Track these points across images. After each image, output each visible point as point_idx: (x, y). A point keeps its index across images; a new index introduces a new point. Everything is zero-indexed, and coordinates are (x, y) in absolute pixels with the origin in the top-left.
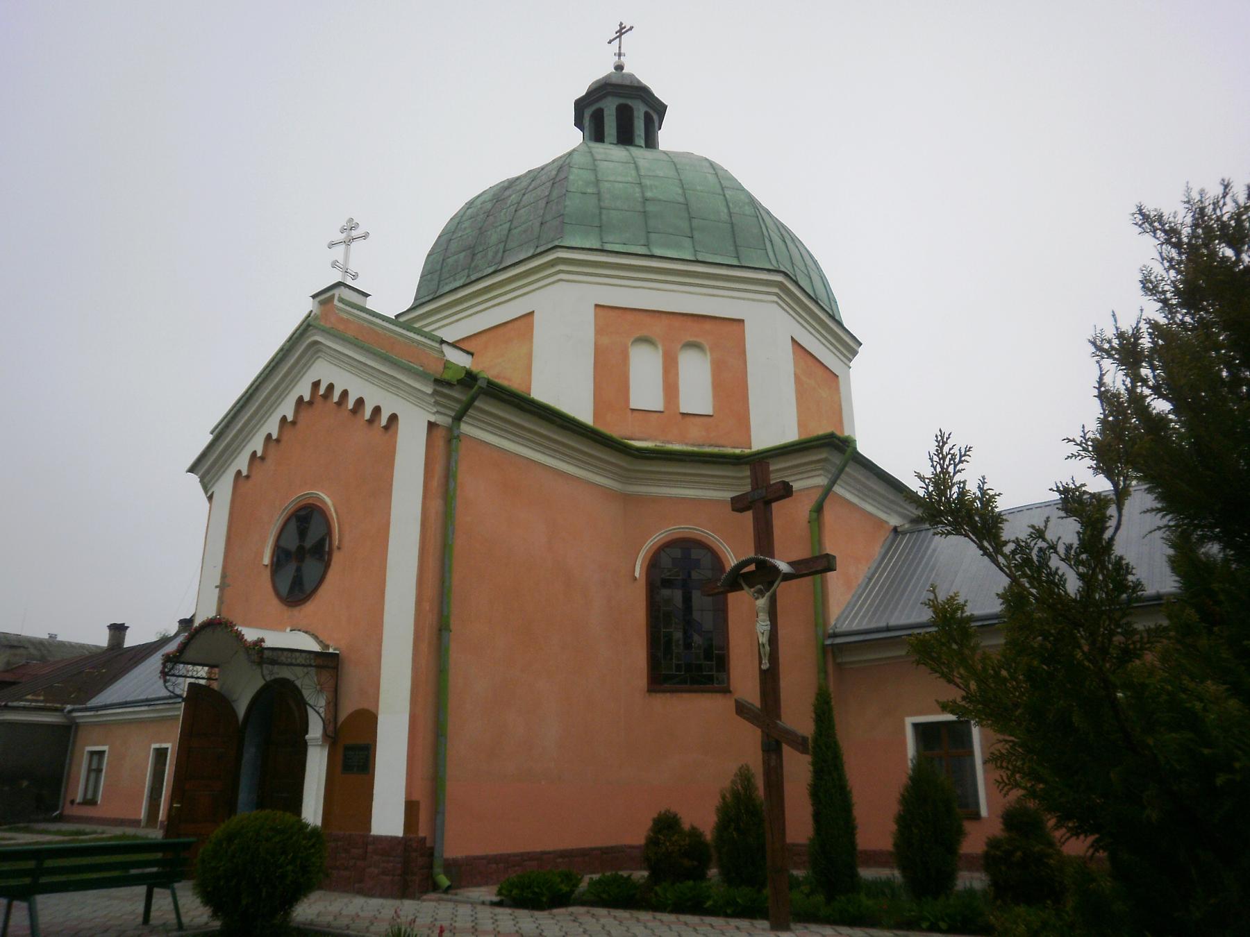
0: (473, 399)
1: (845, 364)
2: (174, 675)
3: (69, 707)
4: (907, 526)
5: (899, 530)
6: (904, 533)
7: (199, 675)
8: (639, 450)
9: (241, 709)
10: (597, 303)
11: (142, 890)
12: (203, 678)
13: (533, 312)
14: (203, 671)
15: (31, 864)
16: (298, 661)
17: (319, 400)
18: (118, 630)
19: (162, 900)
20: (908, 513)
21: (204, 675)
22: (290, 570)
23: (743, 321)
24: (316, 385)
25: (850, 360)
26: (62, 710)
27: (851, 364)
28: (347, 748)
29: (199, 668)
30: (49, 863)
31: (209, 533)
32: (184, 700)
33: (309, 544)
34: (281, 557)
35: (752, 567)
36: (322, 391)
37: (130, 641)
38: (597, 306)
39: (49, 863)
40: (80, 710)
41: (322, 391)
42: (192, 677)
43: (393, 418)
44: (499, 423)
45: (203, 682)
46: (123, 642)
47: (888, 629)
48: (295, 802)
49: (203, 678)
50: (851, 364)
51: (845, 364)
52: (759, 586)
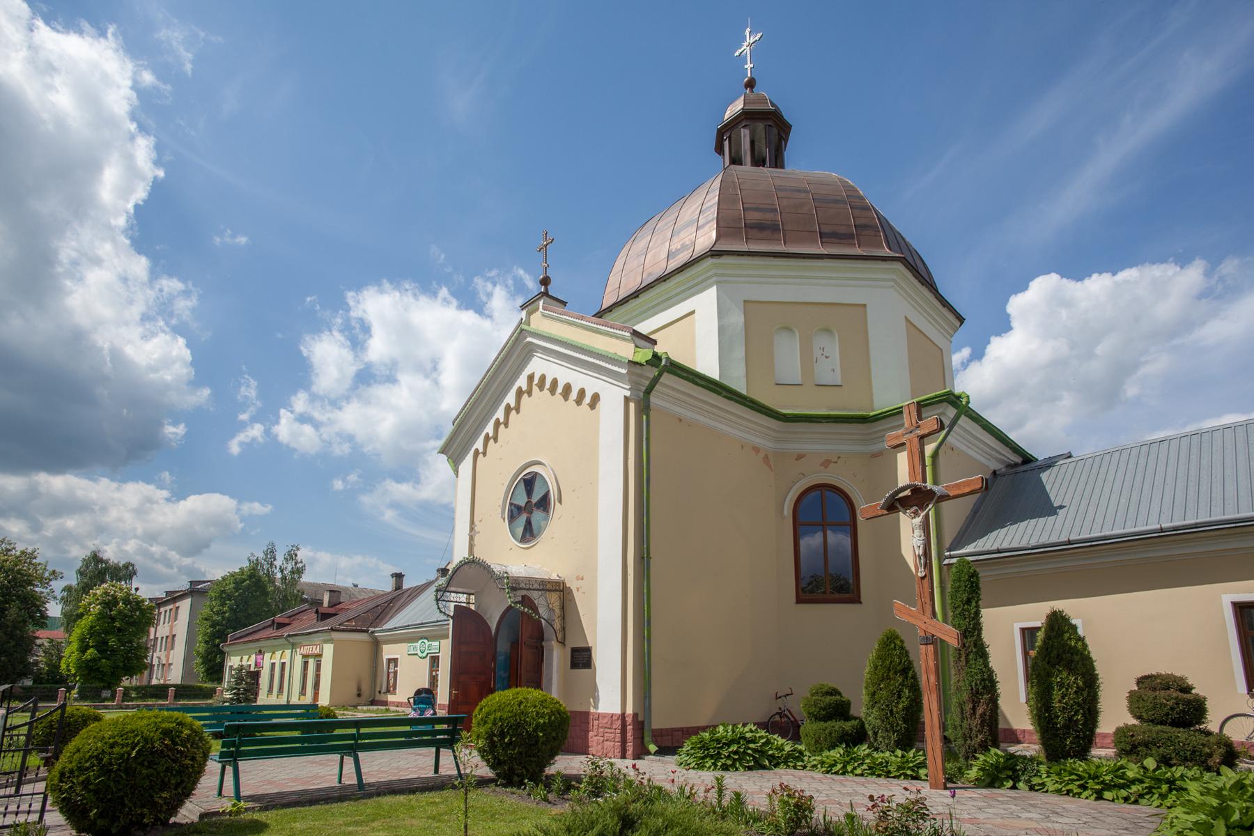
0: (660, 375)
1: (947, 338)
2: (444, 600)
3: (371, 629)
4: (1003, 470)
5: (997, 473)
6: (1003, 475)
7: (461, 600)
8: (785, 415)
9: (493, 627)
10: (746, 299)
11: (434, 749)
12: (464, 603)
13: (694, 311)
14: (463, 598)
15: (354, 731)
16: (534, 587)
17: (535, 389)
18: (399, 577)
19: (446, 757)
20: (1003, 458)
21: (465, 601)
22: (522, 519)
23: (865, 305)
24: (531, 378)
25: (952, 336)
26: (367, 631)
27: (952, 339)
28: (574, 650)
29: (461, 595)
30: (363, 730)
31: (582, 375)
32: (452, 617)
33: (535, 499)
34: (514, 512)
35: (907, 493)
36: (536, 381)
37: (407, 584)
38: (745, 301)
39: (363, 730)
40: (380, 631)
41: (536, 381)
42: (456, 602)
43: (596, 398)
44: (823, 281)
45: (465, 605)
46: (717, 290)
47: (999, 551)
48: (352, 744)
49: (464, 603)
50: (952, 339)
51: (947, 338)
52: (915, 508)
